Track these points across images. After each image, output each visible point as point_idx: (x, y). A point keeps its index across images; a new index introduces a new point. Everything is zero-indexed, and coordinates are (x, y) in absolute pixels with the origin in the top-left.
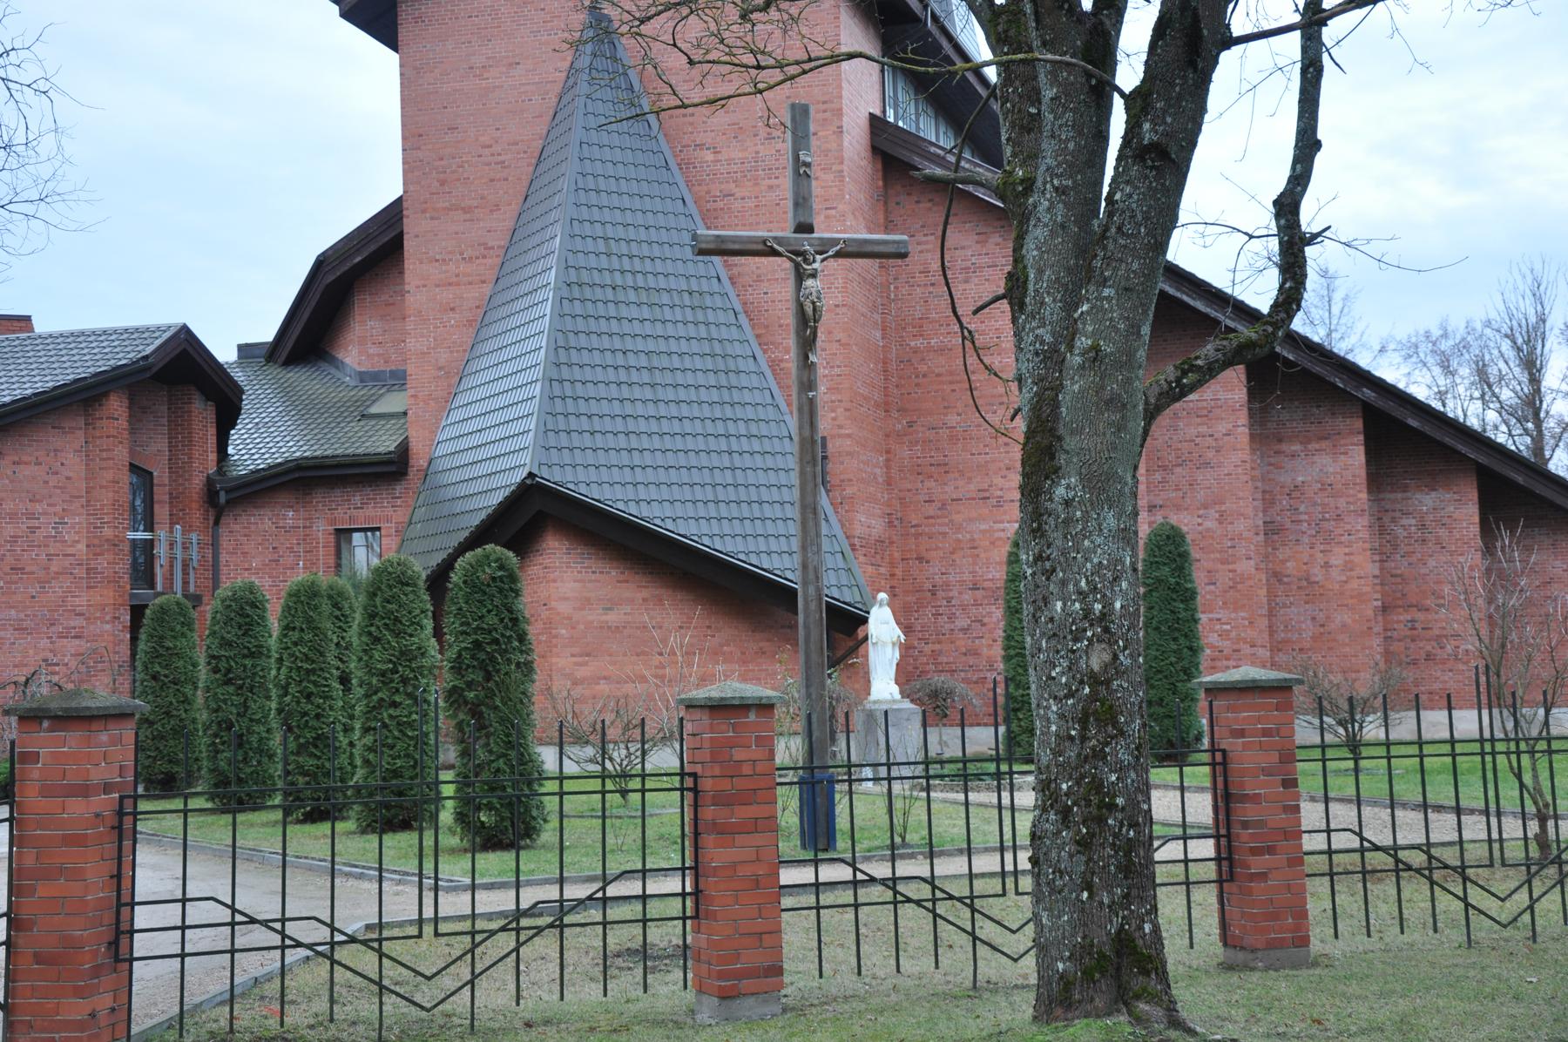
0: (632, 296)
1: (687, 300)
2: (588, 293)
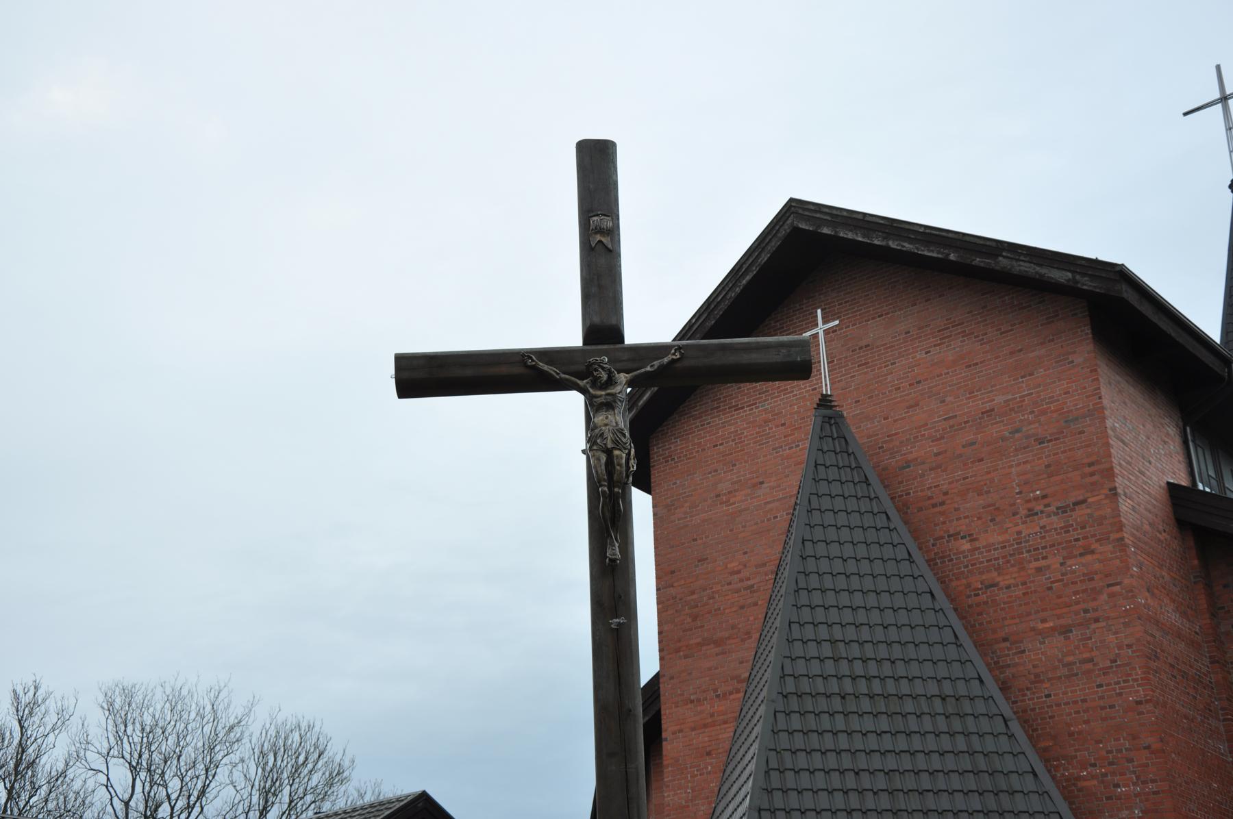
0: (866, 705)
1: (938, 705)
2: (809, 704)
